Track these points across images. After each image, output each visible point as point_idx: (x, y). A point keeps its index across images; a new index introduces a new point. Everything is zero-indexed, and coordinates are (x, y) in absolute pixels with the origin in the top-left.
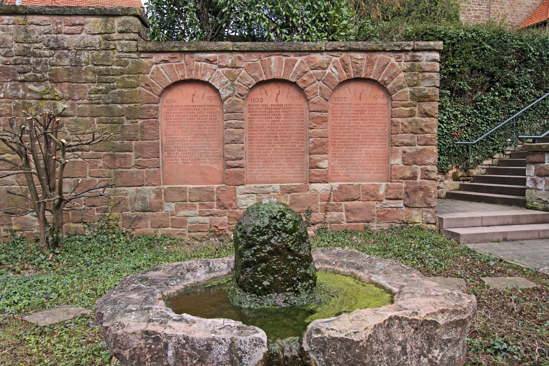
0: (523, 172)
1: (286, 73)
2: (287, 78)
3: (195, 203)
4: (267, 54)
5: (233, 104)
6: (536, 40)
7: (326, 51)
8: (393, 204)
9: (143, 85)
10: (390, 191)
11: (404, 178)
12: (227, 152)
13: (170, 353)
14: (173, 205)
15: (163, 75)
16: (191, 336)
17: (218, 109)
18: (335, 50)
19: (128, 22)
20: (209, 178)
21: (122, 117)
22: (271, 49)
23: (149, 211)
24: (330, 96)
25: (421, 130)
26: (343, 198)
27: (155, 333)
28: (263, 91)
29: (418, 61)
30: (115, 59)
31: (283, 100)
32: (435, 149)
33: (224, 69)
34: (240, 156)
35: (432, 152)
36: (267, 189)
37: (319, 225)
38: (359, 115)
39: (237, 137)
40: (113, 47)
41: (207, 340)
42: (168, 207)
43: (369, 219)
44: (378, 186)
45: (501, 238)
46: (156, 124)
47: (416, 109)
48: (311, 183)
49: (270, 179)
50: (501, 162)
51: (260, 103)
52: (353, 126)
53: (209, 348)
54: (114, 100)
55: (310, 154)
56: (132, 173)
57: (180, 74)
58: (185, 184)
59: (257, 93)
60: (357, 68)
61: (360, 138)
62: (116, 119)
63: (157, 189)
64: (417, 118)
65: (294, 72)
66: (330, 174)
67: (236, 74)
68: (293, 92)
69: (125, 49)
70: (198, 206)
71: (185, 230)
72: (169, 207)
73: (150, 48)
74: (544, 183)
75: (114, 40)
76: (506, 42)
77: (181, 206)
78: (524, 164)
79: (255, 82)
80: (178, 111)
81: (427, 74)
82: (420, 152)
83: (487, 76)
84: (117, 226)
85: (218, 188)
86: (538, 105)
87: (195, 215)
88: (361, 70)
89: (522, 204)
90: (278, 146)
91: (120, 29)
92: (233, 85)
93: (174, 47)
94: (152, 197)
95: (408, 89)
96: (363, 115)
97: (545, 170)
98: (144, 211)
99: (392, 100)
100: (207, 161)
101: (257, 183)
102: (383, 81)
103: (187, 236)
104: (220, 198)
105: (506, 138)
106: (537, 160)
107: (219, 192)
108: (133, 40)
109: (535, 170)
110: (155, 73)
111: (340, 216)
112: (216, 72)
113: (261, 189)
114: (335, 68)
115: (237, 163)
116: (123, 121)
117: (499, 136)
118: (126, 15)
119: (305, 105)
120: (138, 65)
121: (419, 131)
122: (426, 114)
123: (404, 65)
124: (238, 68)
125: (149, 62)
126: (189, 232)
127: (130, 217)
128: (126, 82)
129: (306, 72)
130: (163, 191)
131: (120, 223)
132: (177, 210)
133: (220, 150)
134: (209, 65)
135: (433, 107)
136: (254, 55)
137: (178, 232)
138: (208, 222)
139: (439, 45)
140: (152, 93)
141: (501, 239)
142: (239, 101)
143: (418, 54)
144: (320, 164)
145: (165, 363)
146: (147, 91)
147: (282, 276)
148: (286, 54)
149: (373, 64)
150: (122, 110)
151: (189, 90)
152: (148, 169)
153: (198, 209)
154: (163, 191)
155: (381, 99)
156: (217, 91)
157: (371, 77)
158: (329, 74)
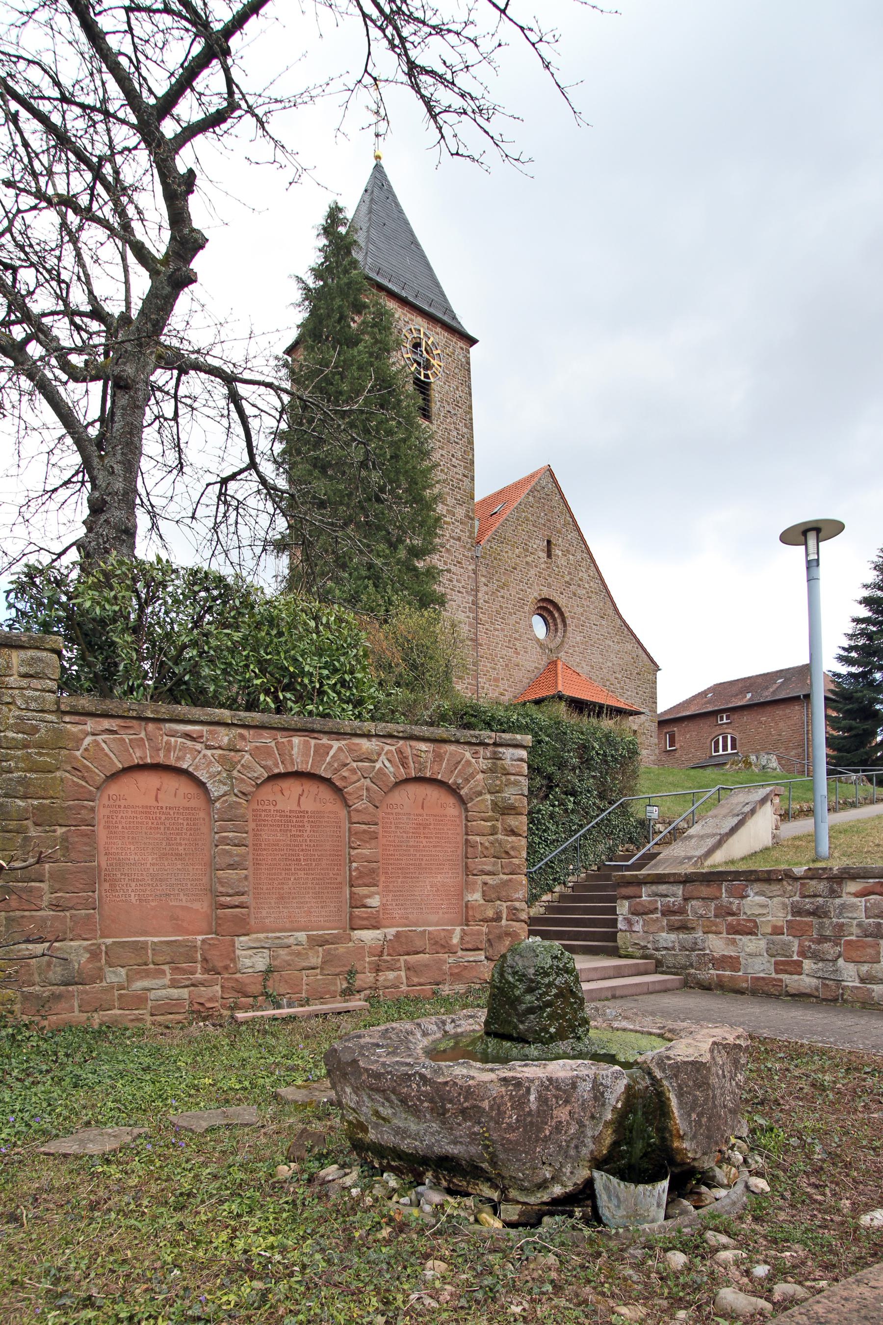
0: (613, 910)
1: (317, 762)
2: (317, 772)
3: (162, 967)
4: (285, 733)
5: (231, 807)
6: (599, 735)
7: (377, 736)
8: (471, 956)
9: (69, 768)
10: (467, 939)
11: (485, 920)
12: (220, 883)
13: (532, 1098)
14: (123, 971)
15: (107, 755)
16: (555, 1076)
17: (202, 815)
18: (391, 736)
19: (40, 660)
20: (185, 924)
21: (25, 822)
22: (293, 726)
23: (76, 984)
24: (381, 801)
25: (507, 853)
26: (401, 950)
27: (514, 1078)
28: (277, 788)
29: (500, 759)
30: (11, 721)
31: (308, 805)
32: (524, 880)
33: (214, 751)
34: (242, 889)
35: (521, 884)
36: (286, 940)
37: (367, 992)
38: (422, 831)
39: (236, 859)
40: (9, 700)
41: (572, 1078)
42: (112, 976)
43: (440, 979)
44: (451, 932)
45: (609, 995)
46: (91, 837)
47: (499, 825)
48: (353, 929)
49: (288, 925)
50: (563, 897)
51: (272, 808)
52: (413, 846)
53: (574, 1086)
54: (10, 792)
55: (351, 886)
56: (44, 919)
57: (138, 755)
58: (142, 935)
59: (268, 793)
60: (420, 763)
61: (423, 863)
62: (13, 825)
63: (92, 945)
64: (500, 836)
65: (329, 763)
66: (381, 916)
67: (236, 760)
68: (325, 793)
69: (33, 705)
70: (168, 971)
71: (144, 1013)
72: (116, 976)
73: (83, 708)
74: (641, 923)
75: (12, 688)
76: (565, 733)
77: (138, 973)
78: (613, 899)
79: (266, 775)
80: (130, 814)
81: (512, 778)
82: (505, 883)
83: (544, 778)
84: (11, 1012)
85: (203, 941)
86: (602, 820)
87: (164, 987)
88: (426, 767)
89: (614, 952)
90: (301, 874)
91: (23, 670)
92: (230, 777)
93: (130, 710)
94: (83, 960)
95: (488, 797)
96: (427, 831)
97: (643, 906)
98: (67, 984)
99: (467, 810)
100: (182, 897)
101: (267, 931)
102: (455, 783)
103: (149, 1023)
104: (209, 957)
105: (568, 864)
106: (632, 894)
107: (207, 947)
108: (49, 691)
109: (630, 907)
110: (91, 749)
111: (398, 977)
112: (201, 755)
113: (277, 941)
114: (390, 761)
115: (237, 900)
116: (27, 828)
117: (561, 861)
118: (37, 648)
119: (343, 813)
120: (59, 734)
121: (504, 855)
122: (513, 832)
123: (483, 764)
124: (239, 751)
125: (81, 731)
126: (152, 1015)
127: (38, 997)
128: (37, 762)
129: (346, 765)
130: (103, 948)
131: (17, 1008)
132: (129, 979)
133: (205, 880)
134: (189, 743)
135: (521, 822)
136: (265, 733)
137: (133, 1017)
138: (186, 997)
139: (528, 739)
140: (84, 784)
141: (610, 996)
142: (240, 803)
143: (501, 749)
144: (369, 902)
145: (527, 1109)
146: (75, 779)
147: (566, 1021)
148: (316, 735)
149: (442, 759)
150: (26, 810)
151: (151, 781)
152: (73, 912)
153: (169, 977)
154: (103, 948)
155: (452, 809)
156: (201, 785)
157: (439, 777)
158: (380, 768)
